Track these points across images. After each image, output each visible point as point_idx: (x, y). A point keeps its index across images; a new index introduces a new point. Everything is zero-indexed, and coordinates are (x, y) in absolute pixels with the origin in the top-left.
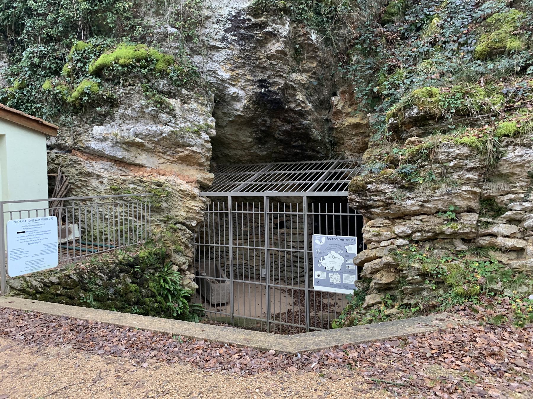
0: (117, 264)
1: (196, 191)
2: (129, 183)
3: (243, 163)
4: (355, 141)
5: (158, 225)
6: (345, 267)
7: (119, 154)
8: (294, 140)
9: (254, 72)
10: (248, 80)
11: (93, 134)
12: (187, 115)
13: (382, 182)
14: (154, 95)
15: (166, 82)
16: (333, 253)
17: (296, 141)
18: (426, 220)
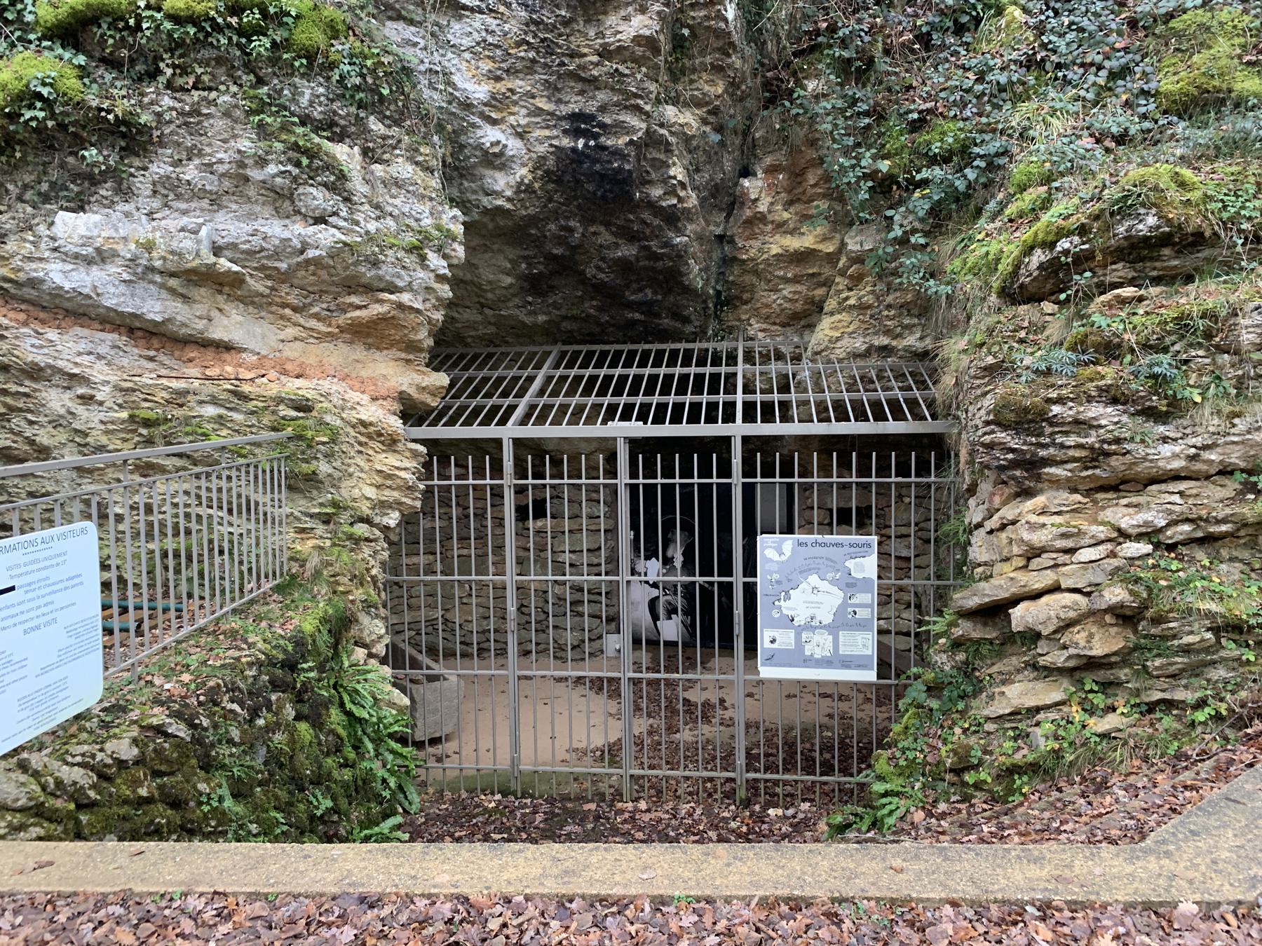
0: (260, 664)
1: (396, 423)
2: (201, 402)
3: (466, 345)
4: (785, 296)
5: (303, 530)
7: (155, 307)
8: (635, 286)
9: (558, 90)
10: (539, 111)
11: (53, 239)
12: (383, 197)
13: (1090, 399)
14: (285, 128)
15: (321, 90)
16: (814, 579)
17: (640, 290)
18: (1194, 491)
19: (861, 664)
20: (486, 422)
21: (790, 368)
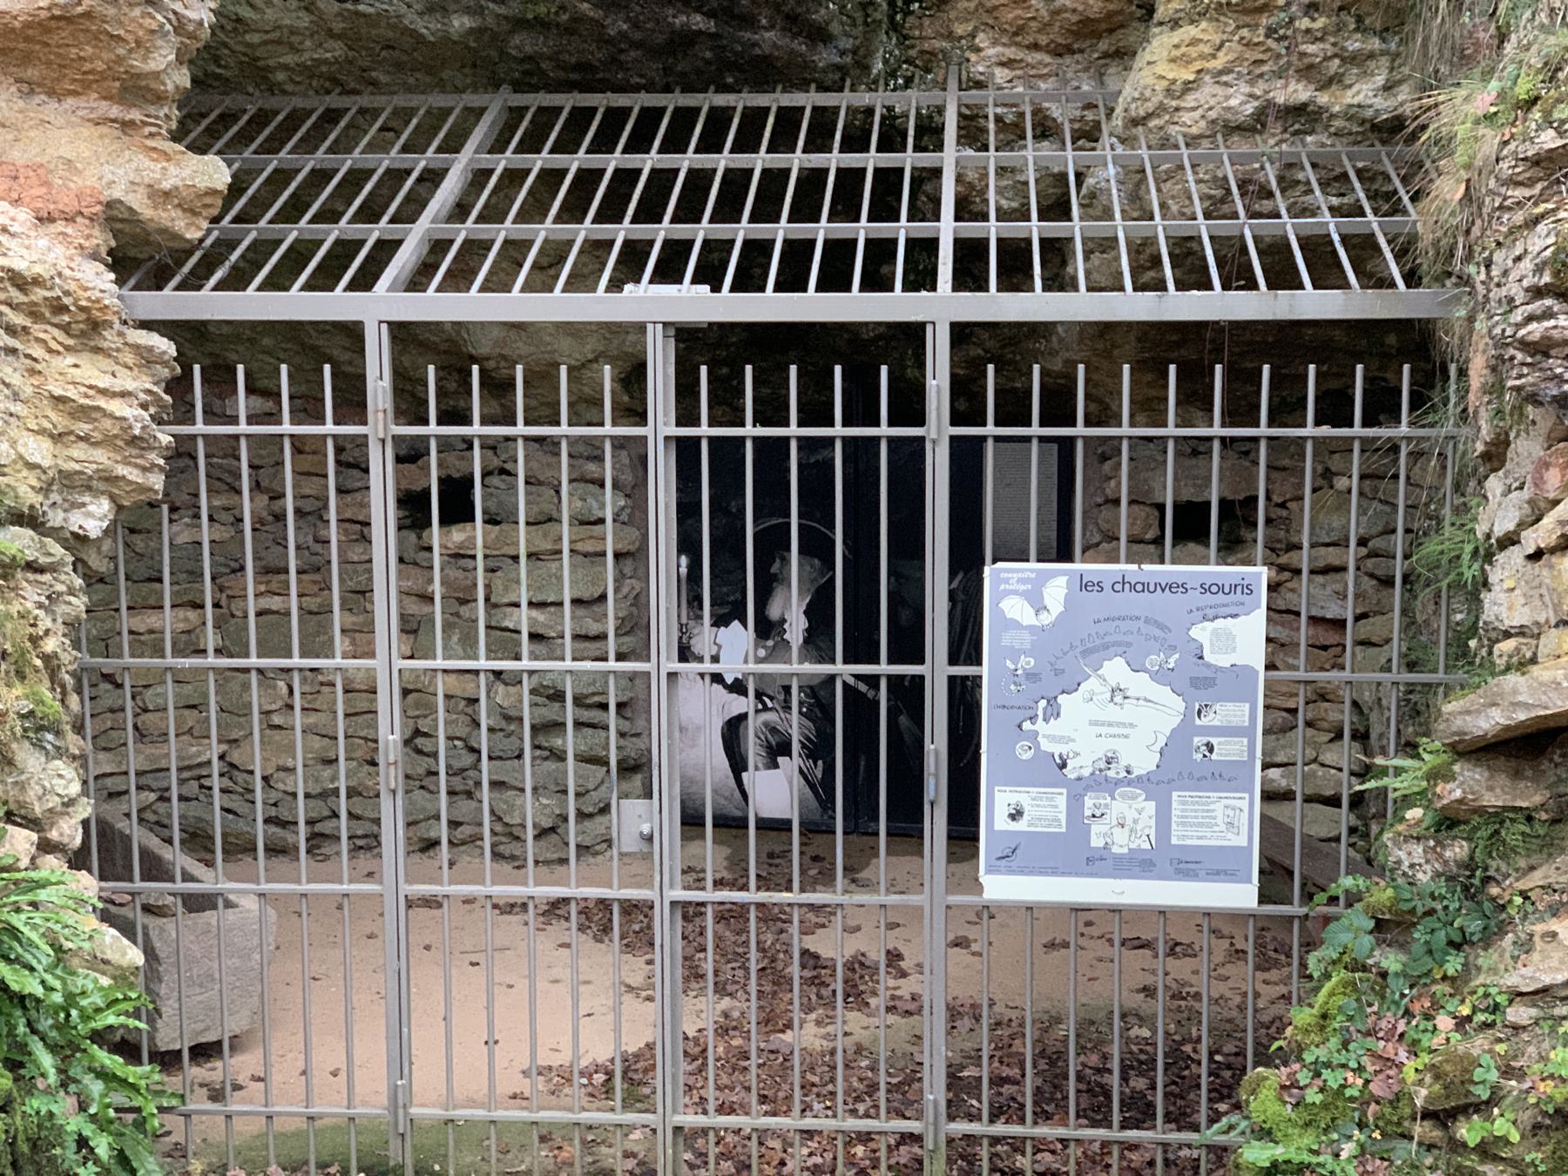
1: (98, 281)
3: (272, 89)
6: (1190, 748)
16: (1115, 669)
20: (324, 280)
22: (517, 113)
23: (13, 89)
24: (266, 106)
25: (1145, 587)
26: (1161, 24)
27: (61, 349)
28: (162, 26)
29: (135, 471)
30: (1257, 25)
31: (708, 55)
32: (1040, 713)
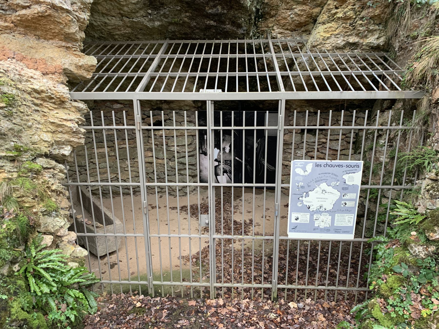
1: (63, 90)
3: (115, 40)
16: (324, 186)
17: (215, 6)
19: (346, 231)
20: (123, 89)
21: (293, 55)
22: (171, 45)
23: (34, 38)
24: (114, 44)
25: (332, 166)
26: (320, 23)
27: (53, 109)
28: (72, 19)
29: (76, 139)
30: (347, 23)
31: (214, 31)
32: (304, 196)
